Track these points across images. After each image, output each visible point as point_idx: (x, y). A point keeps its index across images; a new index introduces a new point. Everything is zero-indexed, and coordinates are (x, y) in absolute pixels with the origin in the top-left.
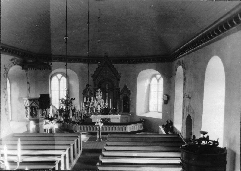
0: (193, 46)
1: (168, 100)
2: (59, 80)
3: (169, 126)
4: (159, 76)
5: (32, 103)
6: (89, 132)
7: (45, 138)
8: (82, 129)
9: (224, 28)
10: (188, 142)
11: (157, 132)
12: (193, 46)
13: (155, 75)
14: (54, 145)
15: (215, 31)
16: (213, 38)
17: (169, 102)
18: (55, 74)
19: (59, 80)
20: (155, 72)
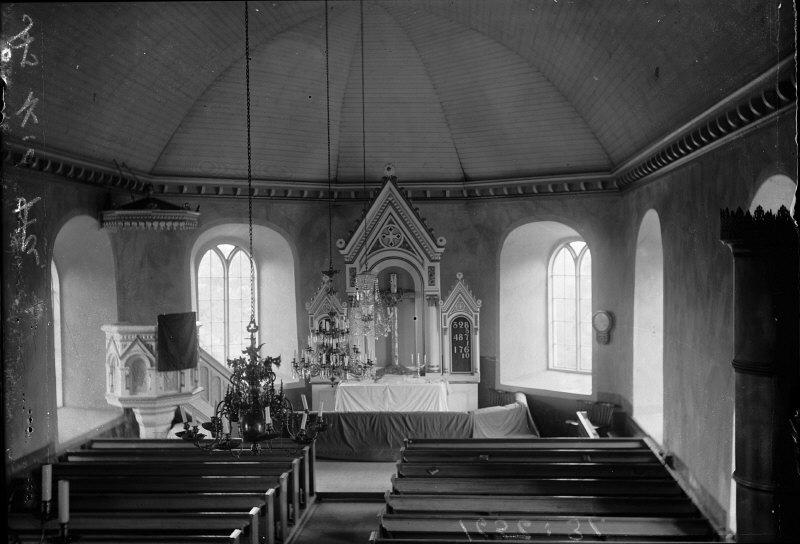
0: (692, 145)
1: (612, 332)
2: (227, 262)
3: (615, 417)
4: (579, 245)
5: (131, 347)
6: (702, 487)
7: (163, 410)
8: (407, 419)
9: (752, 113)
10: (280, 404)
11: (579, 431)
12: (692, 145)
13: (566, 242)
14: (154, 408)
15: (764, 99)
16: (725, 135)
17: (616, 334)
18: (212, 244)
19: (227, 262)
20: (566, 231)
